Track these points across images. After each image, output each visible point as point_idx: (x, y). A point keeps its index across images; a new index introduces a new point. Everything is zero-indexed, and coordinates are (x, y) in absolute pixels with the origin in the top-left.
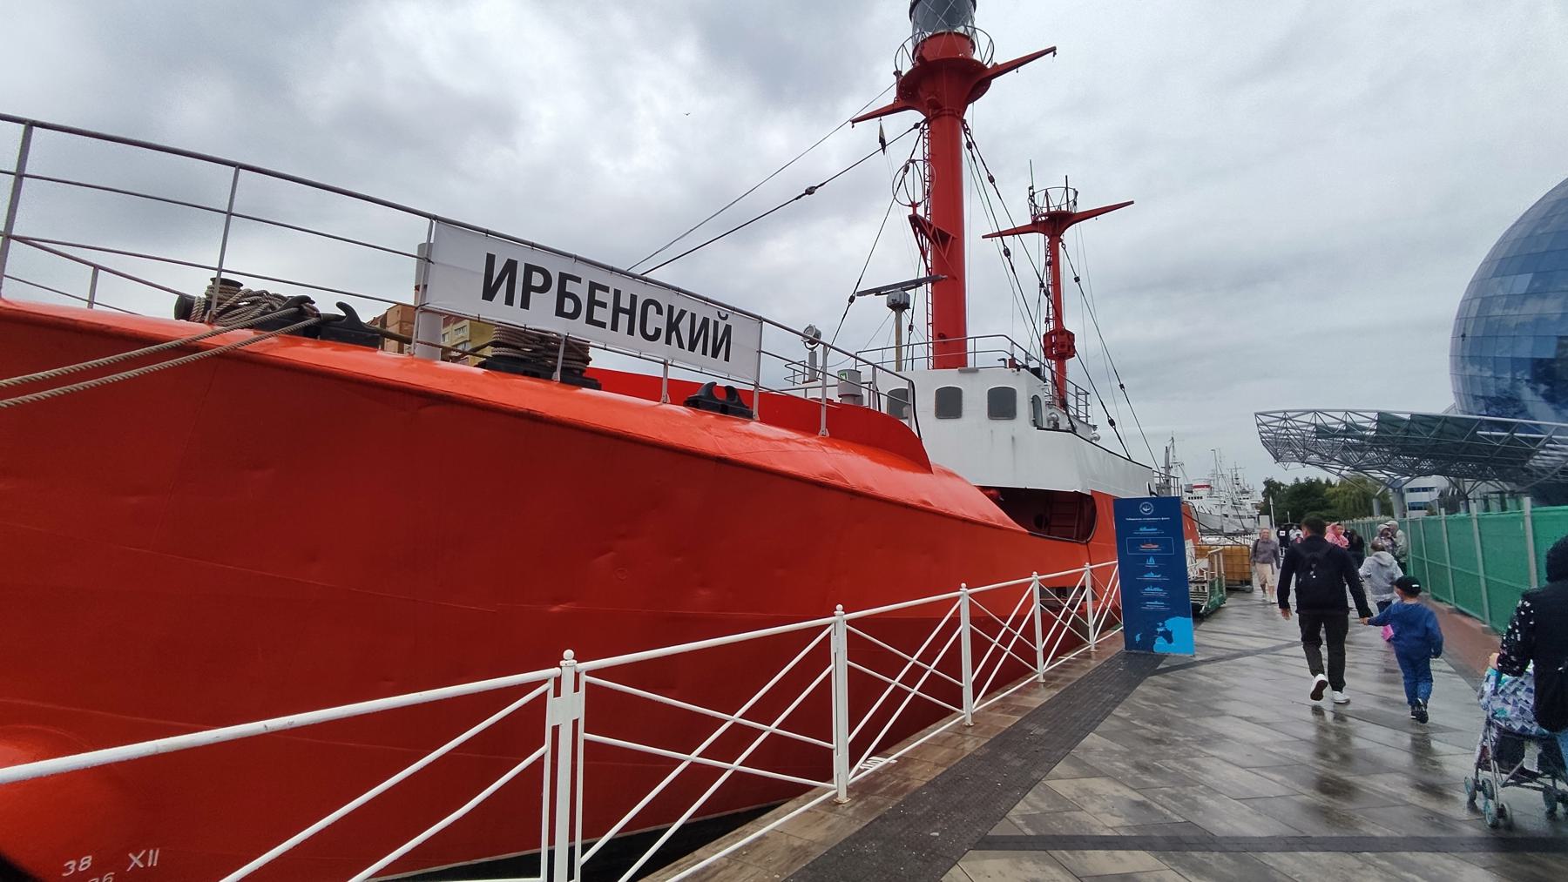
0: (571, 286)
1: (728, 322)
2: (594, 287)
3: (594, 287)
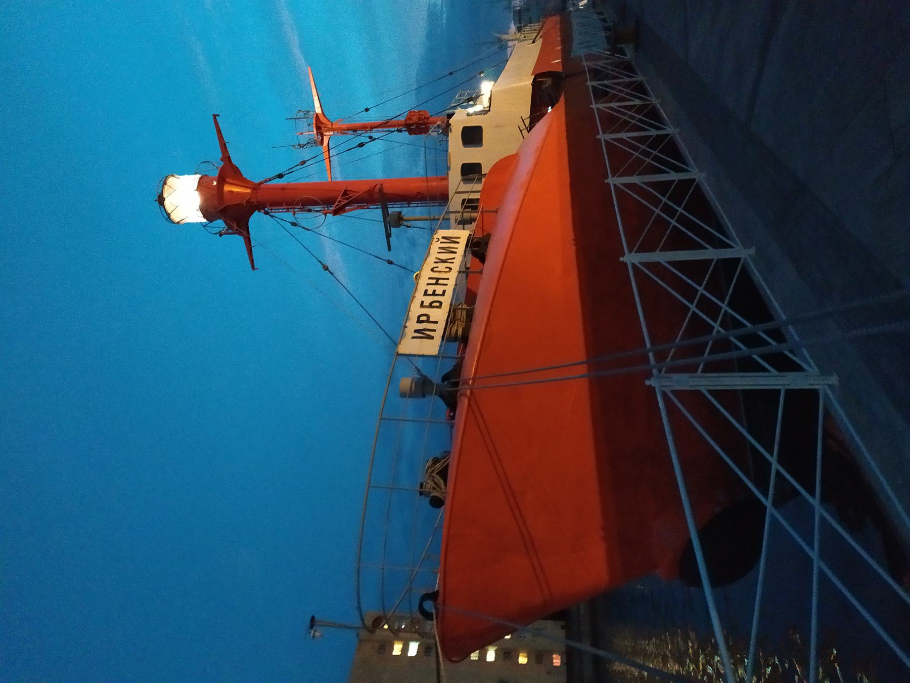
0: (426, 303)
1: (440, 238)
2: (426, 294)
3: (426, 294)
